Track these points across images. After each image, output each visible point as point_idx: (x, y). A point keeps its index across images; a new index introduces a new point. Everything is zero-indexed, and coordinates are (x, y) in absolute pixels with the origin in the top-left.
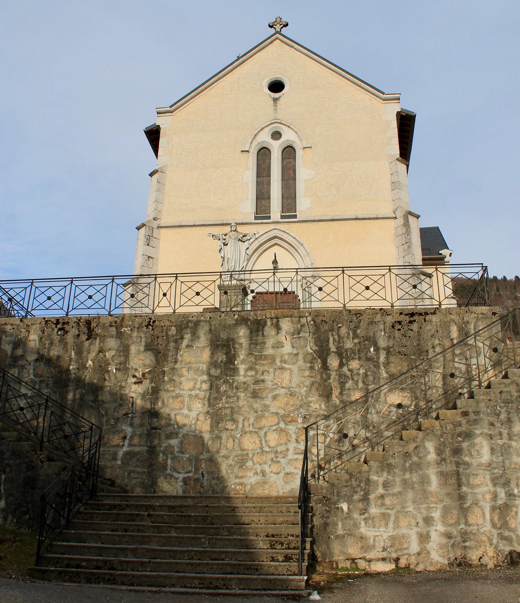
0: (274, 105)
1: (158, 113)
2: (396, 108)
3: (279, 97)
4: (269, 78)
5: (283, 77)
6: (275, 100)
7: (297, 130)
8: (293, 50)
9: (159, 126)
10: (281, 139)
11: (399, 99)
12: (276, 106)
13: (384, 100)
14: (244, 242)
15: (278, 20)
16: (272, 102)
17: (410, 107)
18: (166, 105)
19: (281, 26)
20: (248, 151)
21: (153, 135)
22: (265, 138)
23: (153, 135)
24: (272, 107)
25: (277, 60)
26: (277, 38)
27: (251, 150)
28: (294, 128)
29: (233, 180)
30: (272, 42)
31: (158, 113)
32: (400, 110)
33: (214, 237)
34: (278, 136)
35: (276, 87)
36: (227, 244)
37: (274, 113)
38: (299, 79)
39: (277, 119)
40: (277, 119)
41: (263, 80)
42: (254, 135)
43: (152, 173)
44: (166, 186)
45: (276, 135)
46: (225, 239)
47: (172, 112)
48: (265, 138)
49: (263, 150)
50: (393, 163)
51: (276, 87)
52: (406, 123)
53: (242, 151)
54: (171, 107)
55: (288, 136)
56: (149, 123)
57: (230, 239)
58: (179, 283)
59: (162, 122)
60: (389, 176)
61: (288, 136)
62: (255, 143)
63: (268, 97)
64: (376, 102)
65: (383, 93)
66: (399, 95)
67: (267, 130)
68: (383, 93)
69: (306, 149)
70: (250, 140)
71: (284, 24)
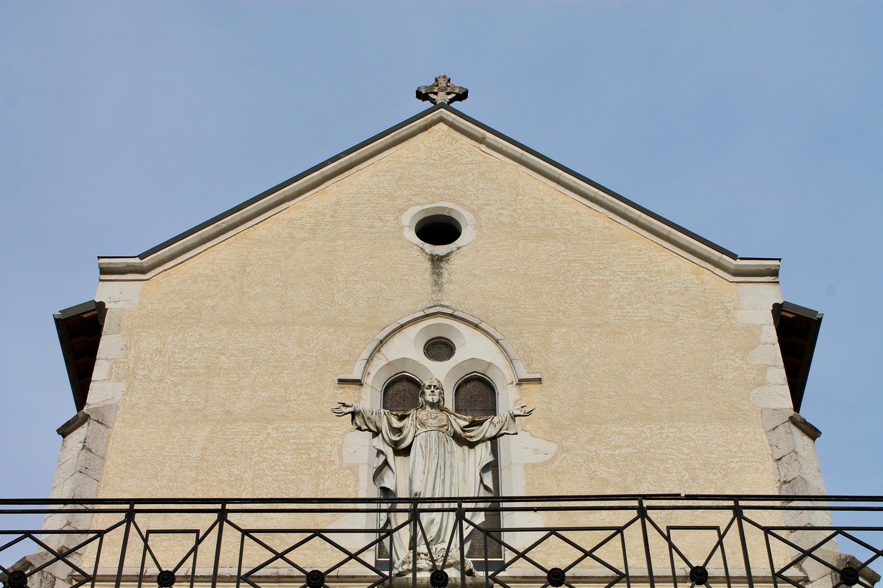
0: (433, 273)
1: (104, 271)
2: (768, 295)
3: (448, 255)
4: (419, 208)
5: (457, 208)
6: (437, 261)
7: (498, 336)
8: (483, 147)
9: (102, 304)
10: (452, 359)
11: (775, 273)
12: (439, 275)
13: (736, 273)
14: (472, 445)
15: (442, 83)
16: (428, 265)
17: (805, 299)
18: (129, 247)
19: (450, 97)
20: (358, 382)
21: (81, 335)
22: (407, 349)
23: (81, 335)
24: (428, 276)
25: (437, 167)
26: (441, 120)
27: (369, 380)
28: (492, 331)
29: (314, 455)
30: (426, 128)
31: (104, 271)
32: (780, 301)
33: (358, 420)
34: (444, 350)
35: (439, 230)
36: (406, 452)
37: (434, 292)
38: (500, 214)
39: (443, 306)
40: (443, 306)
41: (402, 211)
42: (375, 344)
43: (68, 424)
44: (108, 462)
45: (439, 348)
46: (399, 431)
47: (143, 271)
48: (407, 349)
49: (400, 386)
50: (781, 430)
51: (439, 230)
52: (797, 334)
53: (341, 381)
54: (142, 256)
55: (472, 348)
56: (73, 298)
57: (422, 430)
58: (231, 537)
59: (113, 294)
60: (770, 465)
61: (472, 348)
62: (379, 363)
63: (416, 252)
64: (714, 281)
65: (734, 257)
66: (777, 263)
67: (413, 331)
68: (734, 257)
69: (525, 386)
70: (366, 354)
71: (457, 91)
